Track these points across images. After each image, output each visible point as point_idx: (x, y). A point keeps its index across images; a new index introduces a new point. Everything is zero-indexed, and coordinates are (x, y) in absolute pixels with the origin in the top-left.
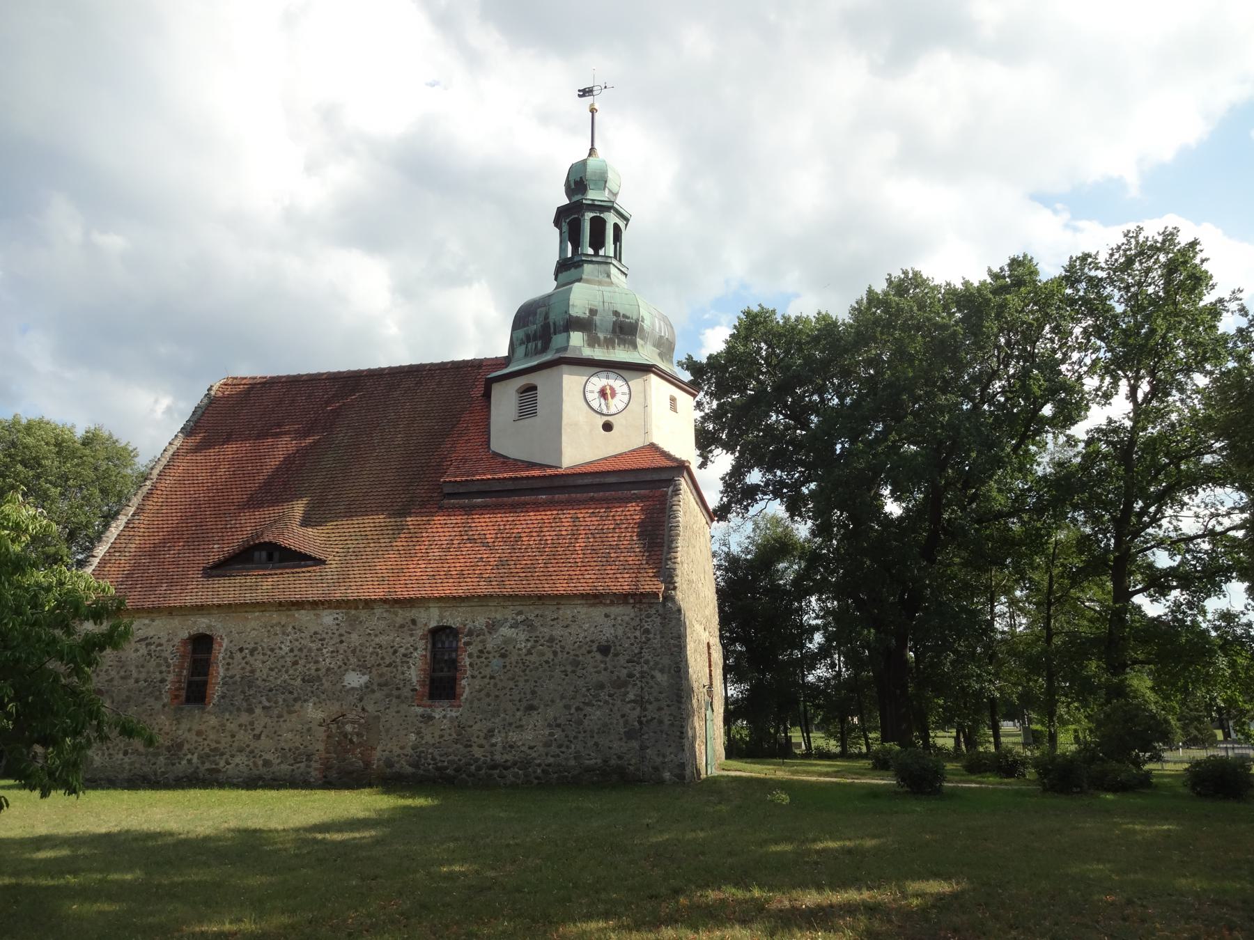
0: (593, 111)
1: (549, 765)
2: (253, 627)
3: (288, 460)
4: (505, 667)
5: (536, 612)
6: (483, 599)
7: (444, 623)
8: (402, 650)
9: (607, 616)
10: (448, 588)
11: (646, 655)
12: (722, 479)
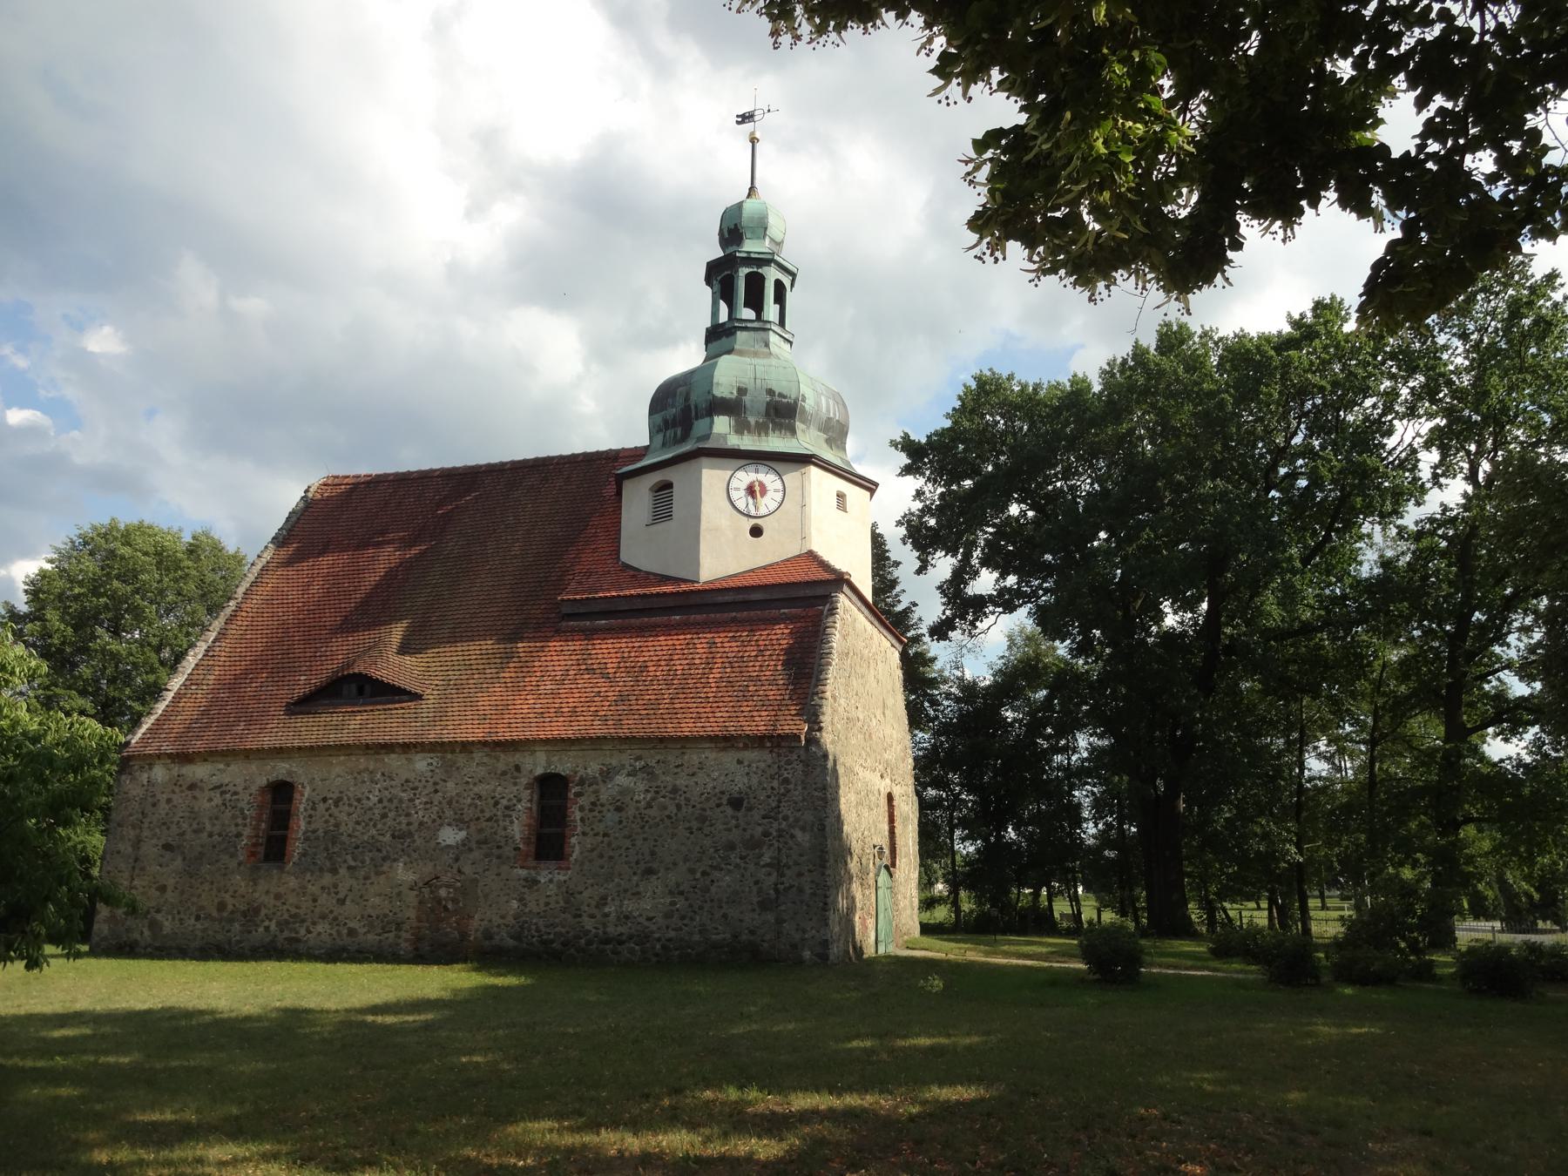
0: (753, 141)
1: (670, 940)
2: (337, 773)
3: (391, 574)
6: (596, 742)
7: (552, 769)
8: (504, 802)
10: (558, 729)
11: (785, 811)
12: (939, 588)
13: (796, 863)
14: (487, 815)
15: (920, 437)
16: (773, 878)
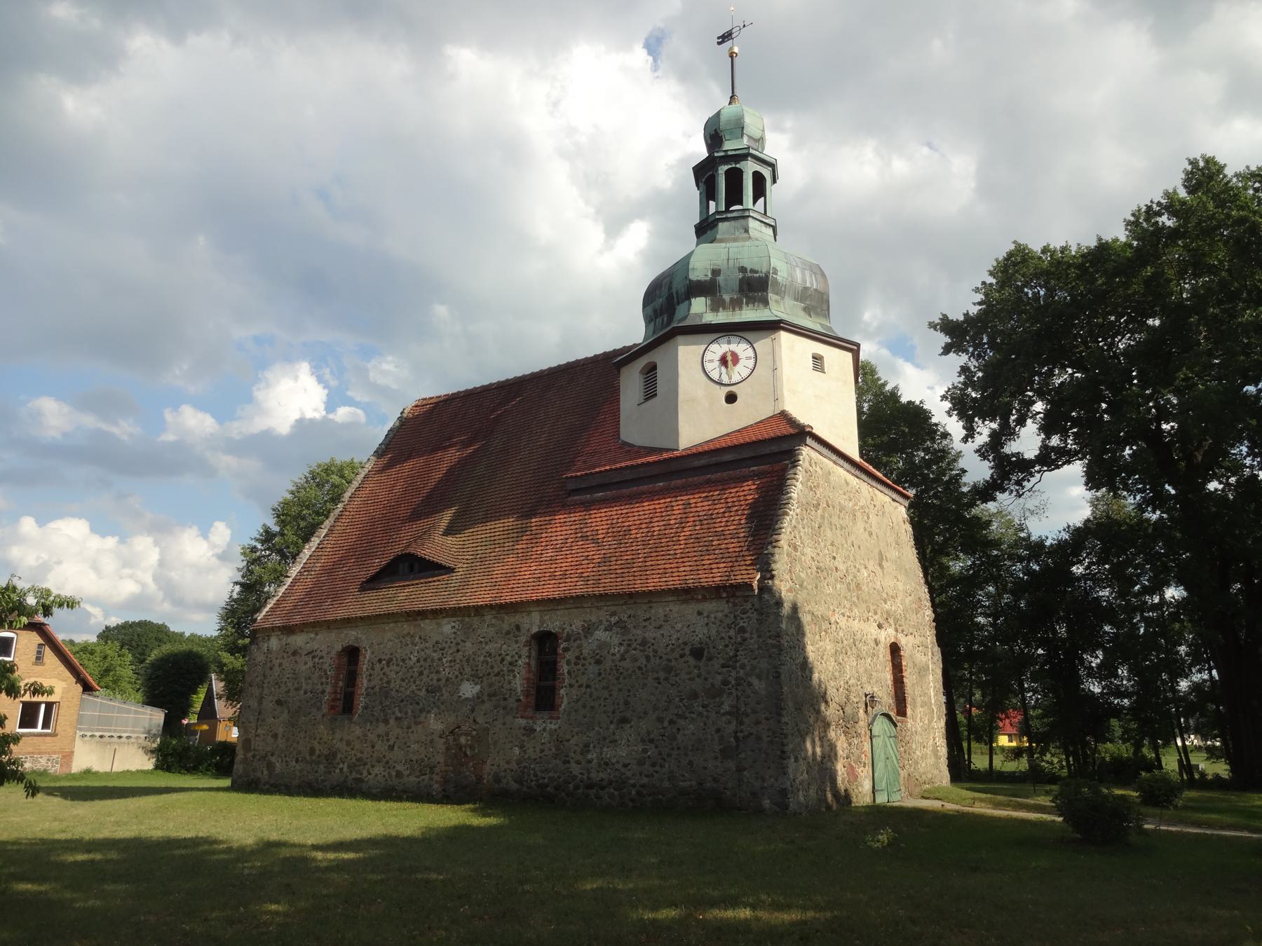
1: (643, 786)
3: (450, 471)
4: (600, 674)
5: (629, 612)
6: (578, 601)
8: (508, 658)
9: (700, 613)
13: (754, 712)
14: (496, 670)
15: (957, 316)
16: (733, 727)
